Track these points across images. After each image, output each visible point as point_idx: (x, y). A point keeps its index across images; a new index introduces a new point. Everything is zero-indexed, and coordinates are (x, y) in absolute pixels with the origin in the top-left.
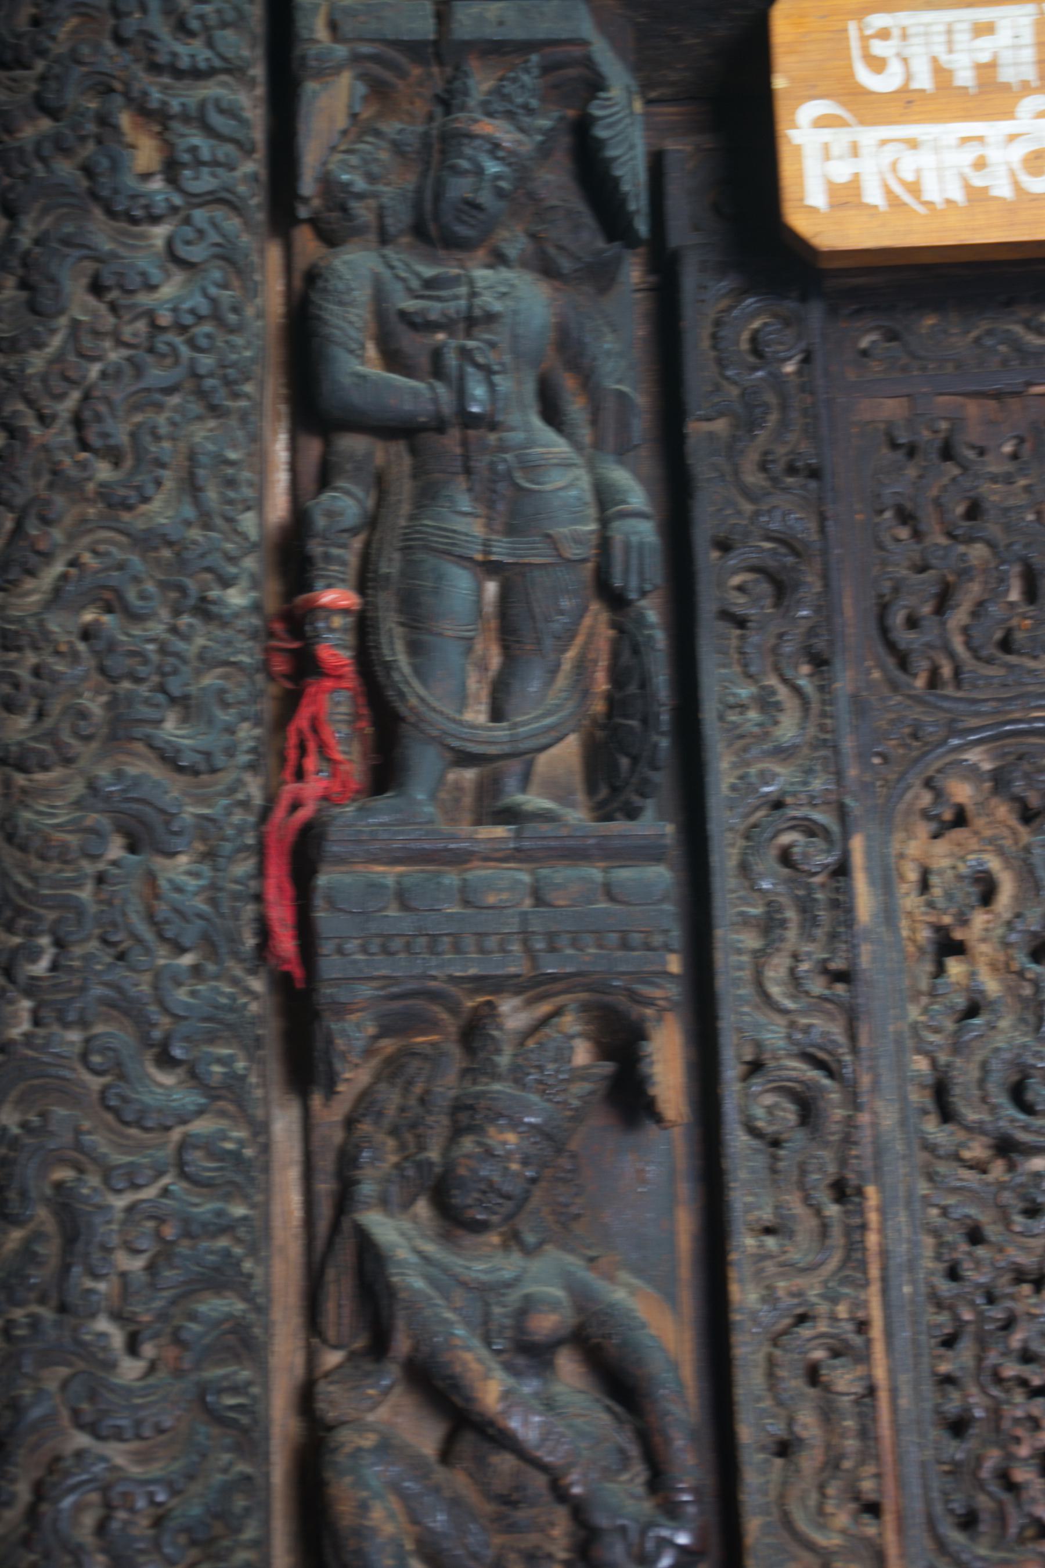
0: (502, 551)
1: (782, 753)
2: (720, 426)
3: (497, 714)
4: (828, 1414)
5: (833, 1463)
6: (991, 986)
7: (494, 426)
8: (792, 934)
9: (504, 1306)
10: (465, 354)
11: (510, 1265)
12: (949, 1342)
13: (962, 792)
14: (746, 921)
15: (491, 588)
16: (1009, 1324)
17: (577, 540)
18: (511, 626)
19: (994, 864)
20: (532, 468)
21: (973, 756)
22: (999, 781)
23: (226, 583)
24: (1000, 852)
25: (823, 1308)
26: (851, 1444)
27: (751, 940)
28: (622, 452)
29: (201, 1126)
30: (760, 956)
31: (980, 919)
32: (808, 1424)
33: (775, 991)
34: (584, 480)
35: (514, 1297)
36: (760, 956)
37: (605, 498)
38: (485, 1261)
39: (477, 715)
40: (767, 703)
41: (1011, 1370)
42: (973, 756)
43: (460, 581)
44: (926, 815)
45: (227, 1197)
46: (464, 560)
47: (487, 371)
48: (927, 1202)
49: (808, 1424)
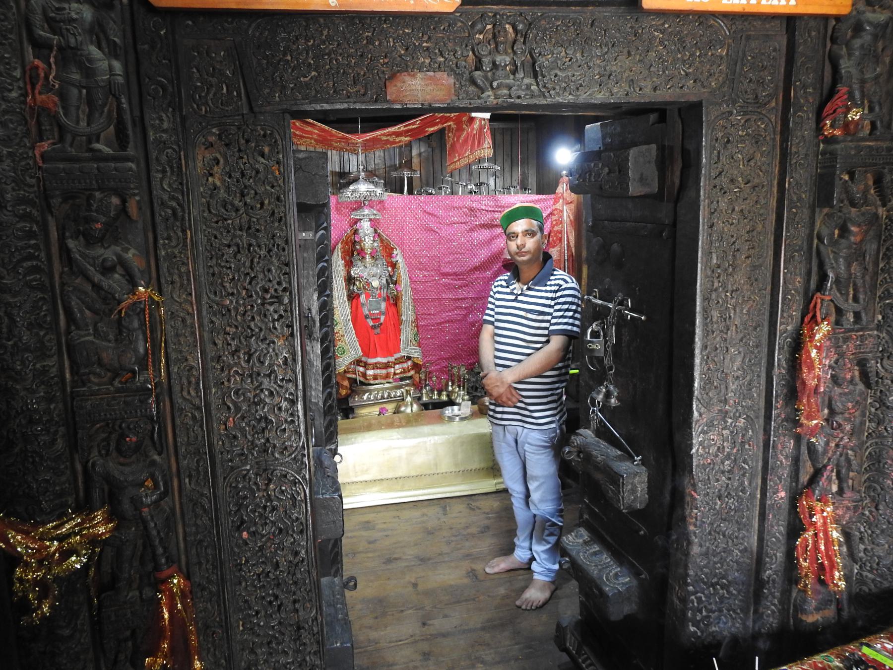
0: (84, 82)
1: (164, 131)
2: (146, 46)
3: (88, 125)
4: (180, 276)
5: (182, 285)
6: (218, 183)
7: (79, 50)
8: (169, 174)
9: (883, 50)
10: (68, 30)
11: (101, 251)
12: (211, 258)
13: (212, 139)
14: (158, 171)
15: (84, 91)
16: (223, 255)
17: (103, 81)
18: (90, 102)
19: (218, 156)
20: (90, 61)
21: (214, 130)
22: (220, 138)
23: (10, 91)
24: (220, 153)
25: (178, 255)
26: (185, 282)
27: (160, 175)
28: (116, 57)
29: (19, 225)
30: (162, 180)
31: (216, 169)
32: (176, 278)
33: (166, 187)
34: (106, 62)
35: (101, 260)
36: (162, 180)
37: (111, 68)
38: (99, 251)
39: (83, 124)
40: (161, 120)
41: (223, 264)
42: (214, 130)
43: (75, 92)
44: (204, 144)
45: (29, 240)
46: (74, 85)
47: (74, 34)
48: (205, 230)
49: (176, 278)
